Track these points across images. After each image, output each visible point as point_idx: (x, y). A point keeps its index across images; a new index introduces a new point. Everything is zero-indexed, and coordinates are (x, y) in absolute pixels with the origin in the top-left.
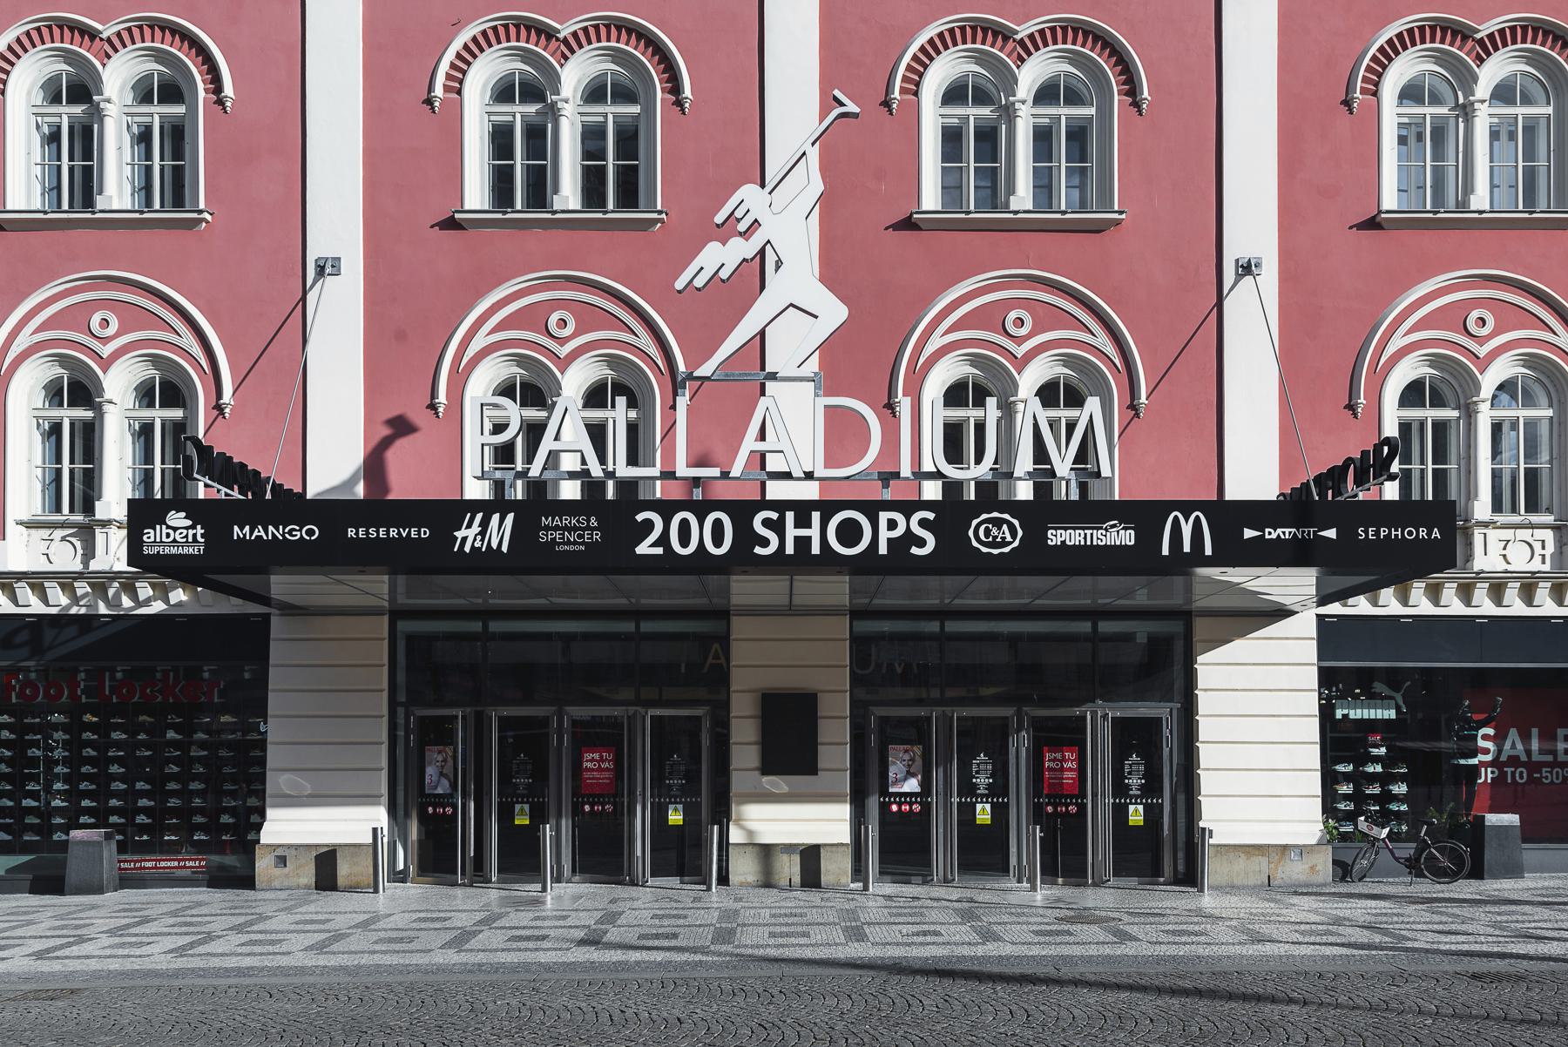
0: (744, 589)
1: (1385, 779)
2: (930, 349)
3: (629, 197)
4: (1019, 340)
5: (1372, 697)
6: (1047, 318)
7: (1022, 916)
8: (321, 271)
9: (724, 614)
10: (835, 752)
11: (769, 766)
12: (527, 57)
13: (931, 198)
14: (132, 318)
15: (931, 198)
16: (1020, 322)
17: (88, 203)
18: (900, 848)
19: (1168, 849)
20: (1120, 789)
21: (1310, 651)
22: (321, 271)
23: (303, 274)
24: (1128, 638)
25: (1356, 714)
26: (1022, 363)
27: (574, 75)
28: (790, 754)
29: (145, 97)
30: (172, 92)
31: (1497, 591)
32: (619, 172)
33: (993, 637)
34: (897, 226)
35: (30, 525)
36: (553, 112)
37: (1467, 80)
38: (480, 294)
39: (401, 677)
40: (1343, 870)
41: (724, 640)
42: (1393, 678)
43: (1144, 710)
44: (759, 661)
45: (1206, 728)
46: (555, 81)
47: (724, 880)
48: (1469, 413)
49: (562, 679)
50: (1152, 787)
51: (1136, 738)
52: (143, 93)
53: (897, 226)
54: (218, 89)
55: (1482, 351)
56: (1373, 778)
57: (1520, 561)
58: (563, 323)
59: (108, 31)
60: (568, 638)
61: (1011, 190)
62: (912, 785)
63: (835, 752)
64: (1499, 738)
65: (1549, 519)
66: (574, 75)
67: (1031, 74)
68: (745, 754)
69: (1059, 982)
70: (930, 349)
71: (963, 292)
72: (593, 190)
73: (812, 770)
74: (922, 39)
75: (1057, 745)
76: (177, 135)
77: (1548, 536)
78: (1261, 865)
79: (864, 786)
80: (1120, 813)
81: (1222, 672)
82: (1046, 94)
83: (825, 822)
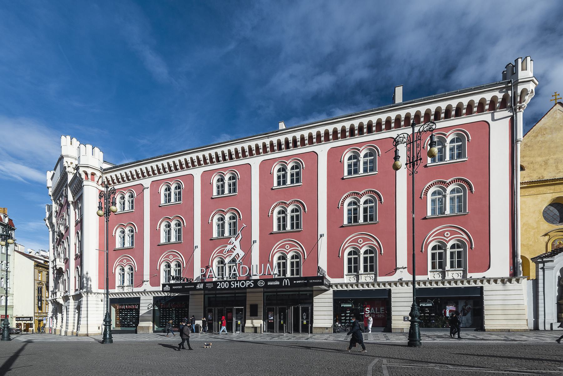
0: (248, 290)
1: (350, 316)
2: (345, 247)
3: (371, 219)
4: (360, 244)
5: (349, 303)
6: (365, 240)
7: (287, 337)
8: (321, 236)
9: (246, 293)
10: (261, 312)
11: (251, 315)
12: (283, 207)
13: (429, 214)
14: (174, 256)
15: (429, 214)
16: (447, 234)
17: (223, 235)
18: (270, 327)
19: (308, 328)
20: (302, 318)
21: (332, 296)
22: (321, 236)
23: (192, 248)
24: (306, 294)
25: (345, 306)
26: (448, 242)
27: (289, 209)
28: (254, 314)
29: (219, 220)
30: (234, 218)
31: (475, 282)
32: (370, 217)
33: (286, 295)
34: (423, 219)
35: (430, 272)
36: (286, 215)
37: (445, 190)
38: (431, 230)
39: (265, 302)
40: (334, 332)
41: (246, 296)
42: (432, 299)
43: (306, 306)
44: (251, 299)
45: (315, 309)
46: (359, 201)
47: (311, 333)
48: (445, 250)
49: (225, 303)
50: (307, 318)
51: (305, 310)
52: (230, 218)
53: (423, 219)
54: (305, 210)
55: (361, 246)
56: (347, 316)
57: (456, 277)
58: (361, 241)
59: (288, 203)
60: (227, 297)
61: (445, 210)
62: (272, 318)
63: (261, 312)
64: (370, 310)
65: (462, 269)
66: (289, 209)
67: (449, 189)
68: (248, 314)
69: (500, 357)
70: (345, 247)
71: (437, 229)
72: (365, 219)
73: (257, 316)
74: (272, 207)
75: (229, 312)
76: (235, 223)
77: (461, 272)
78: (321, 330)
79: (265, 318)
80: (302, 322)
81: (317, 300)
82: (366, 202)
83: (259, 323)
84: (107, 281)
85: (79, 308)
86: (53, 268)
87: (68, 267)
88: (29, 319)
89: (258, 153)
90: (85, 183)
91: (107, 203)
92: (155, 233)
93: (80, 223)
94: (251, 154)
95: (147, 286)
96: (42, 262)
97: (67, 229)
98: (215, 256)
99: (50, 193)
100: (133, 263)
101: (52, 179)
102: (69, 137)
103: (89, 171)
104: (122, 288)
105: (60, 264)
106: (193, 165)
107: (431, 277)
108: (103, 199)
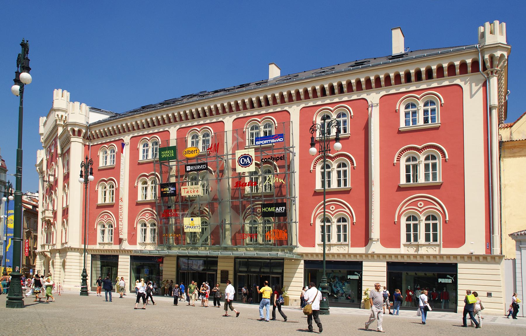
16: (421, 204)
35: (404, 245)
84: (88, 235)
85: (64, 265)
86: (42, 219)
87: (55, 217)
88: (54, 243)
89: (231, 110)
90: (72, 139)
91: (87, 172)
92: (133, 191)
93: (66, 177)
94: (170, 122)
95: (376, 248)
96: (31, 207)
97: (56, 181)
98: (139, 218)
99: (42, 140)
100: (112, 219)
101: (45, 124)
102: (60, 91)
103: (76, 129)
104: (103, 243)
105: (49, 214)
106: (170, 122)
107: (404, 251)
108: (83, 168)
